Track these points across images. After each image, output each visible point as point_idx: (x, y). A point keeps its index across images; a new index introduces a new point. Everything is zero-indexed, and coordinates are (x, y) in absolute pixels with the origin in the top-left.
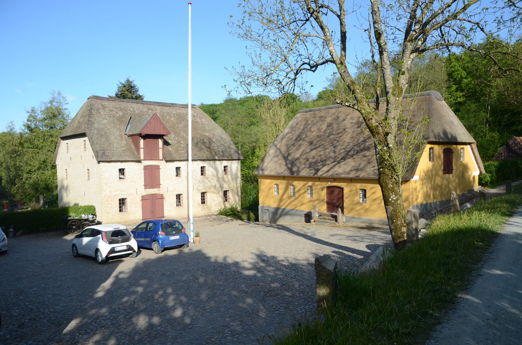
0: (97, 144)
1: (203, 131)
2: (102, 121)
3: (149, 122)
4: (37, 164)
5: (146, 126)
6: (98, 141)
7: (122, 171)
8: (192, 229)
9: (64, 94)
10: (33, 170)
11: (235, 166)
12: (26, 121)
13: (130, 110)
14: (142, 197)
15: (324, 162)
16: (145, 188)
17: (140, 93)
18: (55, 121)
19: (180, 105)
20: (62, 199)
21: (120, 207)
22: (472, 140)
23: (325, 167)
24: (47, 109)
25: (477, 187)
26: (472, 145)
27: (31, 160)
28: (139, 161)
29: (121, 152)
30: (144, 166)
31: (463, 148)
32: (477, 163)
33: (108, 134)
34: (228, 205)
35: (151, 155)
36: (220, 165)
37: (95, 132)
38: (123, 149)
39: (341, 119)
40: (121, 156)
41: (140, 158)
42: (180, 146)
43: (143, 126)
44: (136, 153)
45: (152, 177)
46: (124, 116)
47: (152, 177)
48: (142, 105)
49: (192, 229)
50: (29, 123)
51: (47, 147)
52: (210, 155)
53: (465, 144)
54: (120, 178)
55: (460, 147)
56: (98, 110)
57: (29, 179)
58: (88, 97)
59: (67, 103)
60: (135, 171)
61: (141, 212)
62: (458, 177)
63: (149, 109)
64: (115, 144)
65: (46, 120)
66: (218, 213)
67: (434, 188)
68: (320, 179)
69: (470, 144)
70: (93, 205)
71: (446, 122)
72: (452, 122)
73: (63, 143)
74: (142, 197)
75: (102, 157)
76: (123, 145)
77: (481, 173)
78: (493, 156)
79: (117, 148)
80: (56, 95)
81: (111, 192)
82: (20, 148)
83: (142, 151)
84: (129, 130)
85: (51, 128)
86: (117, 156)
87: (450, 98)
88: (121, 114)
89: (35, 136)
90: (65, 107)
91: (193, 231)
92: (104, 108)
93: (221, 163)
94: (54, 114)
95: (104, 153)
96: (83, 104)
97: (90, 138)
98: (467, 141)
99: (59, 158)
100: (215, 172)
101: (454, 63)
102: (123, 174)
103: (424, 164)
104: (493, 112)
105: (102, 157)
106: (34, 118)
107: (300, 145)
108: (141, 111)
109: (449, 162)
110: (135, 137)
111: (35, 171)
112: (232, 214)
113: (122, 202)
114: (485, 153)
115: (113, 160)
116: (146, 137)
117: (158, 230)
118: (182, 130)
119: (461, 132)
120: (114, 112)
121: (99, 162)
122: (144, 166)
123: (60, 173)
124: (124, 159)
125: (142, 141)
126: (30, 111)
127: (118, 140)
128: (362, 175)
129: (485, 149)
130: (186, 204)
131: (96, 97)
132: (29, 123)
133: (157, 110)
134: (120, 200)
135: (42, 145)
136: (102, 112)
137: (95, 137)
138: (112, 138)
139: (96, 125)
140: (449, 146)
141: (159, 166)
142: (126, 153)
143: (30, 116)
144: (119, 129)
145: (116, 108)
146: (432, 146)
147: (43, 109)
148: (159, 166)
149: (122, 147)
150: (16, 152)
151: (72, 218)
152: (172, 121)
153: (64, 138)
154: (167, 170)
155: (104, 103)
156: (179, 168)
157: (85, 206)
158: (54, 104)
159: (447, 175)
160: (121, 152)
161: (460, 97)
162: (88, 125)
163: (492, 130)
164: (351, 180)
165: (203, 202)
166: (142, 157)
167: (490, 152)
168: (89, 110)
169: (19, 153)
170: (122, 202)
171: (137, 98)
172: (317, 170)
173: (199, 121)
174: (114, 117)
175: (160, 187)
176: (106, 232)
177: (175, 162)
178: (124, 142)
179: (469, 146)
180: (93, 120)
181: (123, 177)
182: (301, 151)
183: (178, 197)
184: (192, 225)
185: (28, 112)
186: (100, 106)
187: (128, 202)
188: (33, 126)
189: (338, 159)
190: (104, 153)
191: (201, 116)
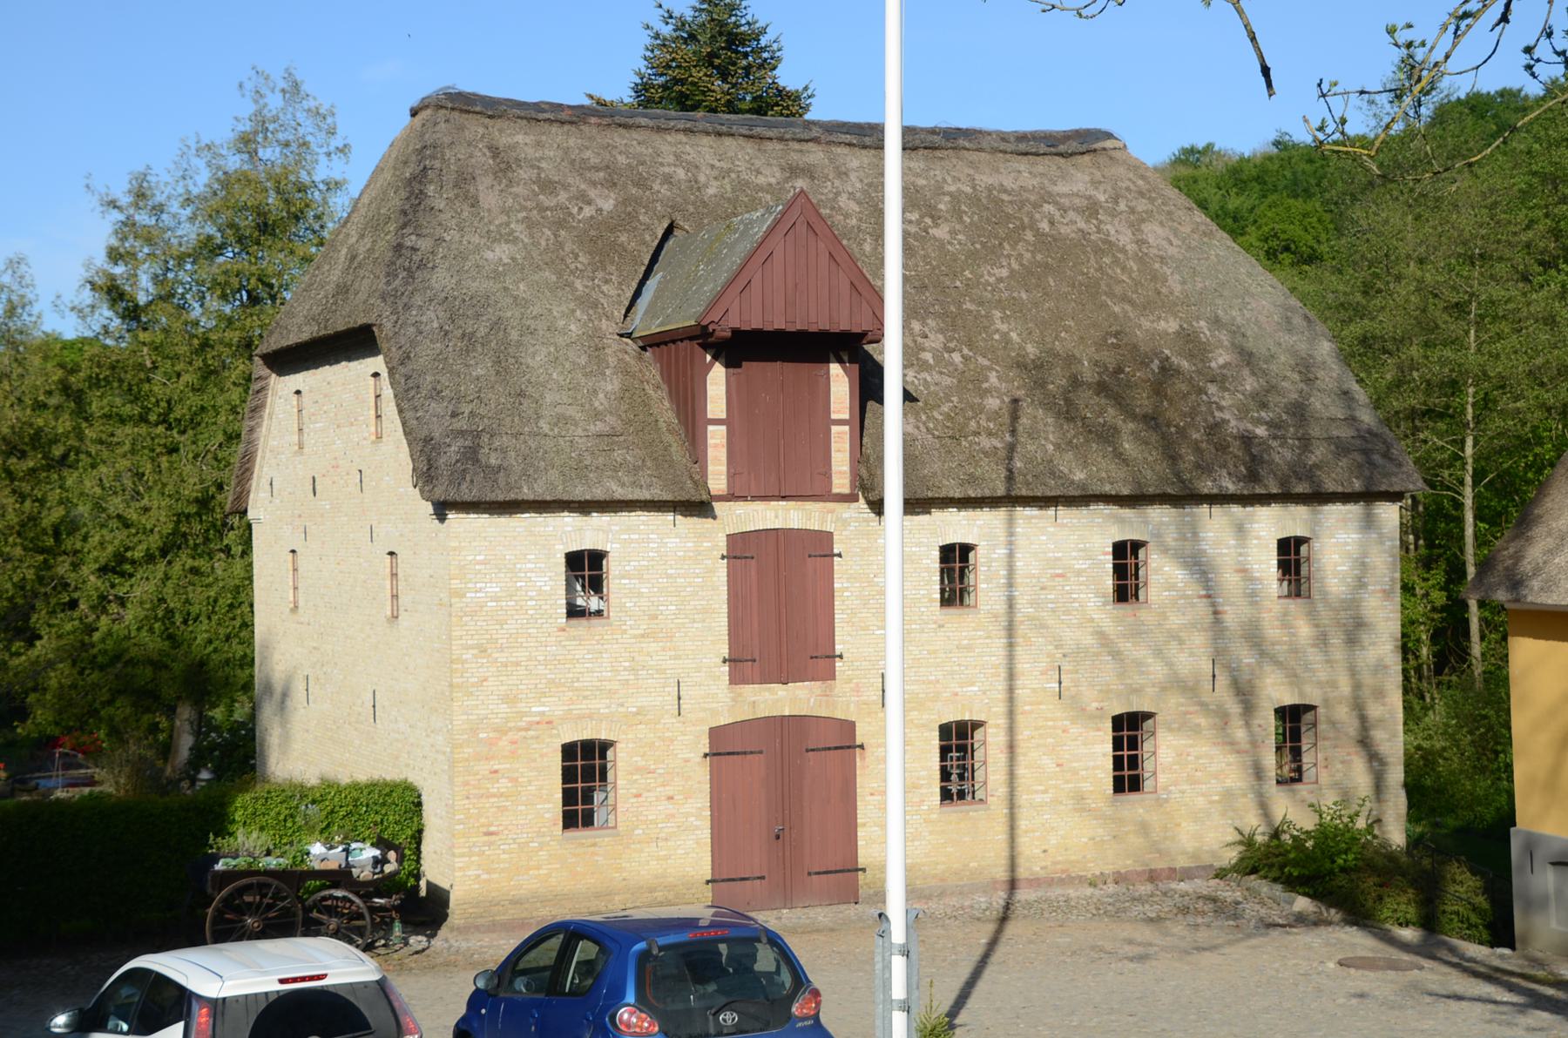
0: (436, 394)
1: (1146, 307)
2: (488, 248)
3: (760, 253)
4: (160, 518)
5: (739, 280)
6: (445, 380)
7: (586, 568)
8: (898, 991)
9: (320, 93)
10: (138, 554)
11: (1356, 547)
12: (101, 260)
13: (668, 179)
14: (715, 733)
16: (735, 679)
17: (787, 77)
18: (272, 259)
19: (1003, 137)
21: (569, 797)
24: (227, 182)
27: (109, 491)
28: (699, 507)
29: (582, 443)
30: (732, 539)
33: (514, 335)
34: (1296, 813)
35: (780, 465)
36: (1247, 539)
37: (433, 318)
38: (599, 427)
40: (581, 470)
41: (701, 482)
42: (979, 410)
43: (724, 277)
44: (677, 451)
45: (781, 609)
46: (625, 219)
47: (781, 609)
48: (750, 147)
49: (898, 991)
50: (119, 270)
51: (222, 419)
52: (1163, 468)
54: (574, 612)
56: (464, 179)
57: (114, 608)
58: (414, 101)
59: (344, 150)
60: (672, 569)
61: (706, 835)
63: (794, 171)
64: (549, 398)
65: (218, 250)
66: (1232, 856)
70: (414, 778)
73: (282, 388)
74: (715, 733)
75: (459, 477)
76: (600, 402)
79: (562, 420)
80: (274, 102)
81: (510, 699)
82: (64, 424)
83: (716, 437)
84: (651, 312)
85: (254, 300)
86: (553, 474)
88: (608, 205)
89: (156, 348)
90: (322, 171)
91: (906, 1007)
92: (504, 164)
93: (1240, 530)
94: (262, 218)
95: (472, 455)
96: (384, 148)
97: (396, 354)
99: (265, 483)
100: (1194, 590)
102: (596, 585)
105: (463, 478)
106: (149, 241)
108: (742, 185)
110: (684, 347)
111: (150, 558)
112: (1319, 874)
113: (585, 767)
115: (526, 493)
116: (740, 348)
117: (617, 998)
118: (999, 304)
120: (563, 197)
121: (442, 509)
122: (732, 539)
123: (1548, 503)
124: (598, 494)
125: (717, 378)
126: (125, 200)
127: (571, 364)
130: (1002, 791)
131: (461, 103)
132: (119, 270)
133: (842, 174)
134: (569, 751)
135: (194, 400)
136: (489, 198)
137: (426, 352)
138: (537, 358)
139: (441, 279)
141: (827, 537)
142: (618, 455)
143: (128, 227)
144: (590, 303)
145: (582, 167)
147: (202, 180)
148: (827, 537)
149: (597, 416)
150: (38, 440)
151: (241, 862)
152: (942, 245)
153: (291, 359)
154: (882, 561)
155: (503, 141)
156: (966, 549)
157: (356, 786)
158: (266, 153)
160: (582, 443)
162: (392, 275)
165: (1128, 778)
166: (717, 480)
168: (409, 182)
169: (57, 451)
170: (585, 767)
171: (761, 107)
173: (1125, 239)
174: (560, 224)
175: (831, 675)
176: (218, 1007)
177: (937, 515)
178: (612, 385)
180: (424, 245)
181: (594, 603)
183: (957, 741)
184: (898, 964)
185: (113, 204)
186: (482, 158)
187: (621, 763)
188: (144, 290)
190: (472, 455)
191: (1142, 205)
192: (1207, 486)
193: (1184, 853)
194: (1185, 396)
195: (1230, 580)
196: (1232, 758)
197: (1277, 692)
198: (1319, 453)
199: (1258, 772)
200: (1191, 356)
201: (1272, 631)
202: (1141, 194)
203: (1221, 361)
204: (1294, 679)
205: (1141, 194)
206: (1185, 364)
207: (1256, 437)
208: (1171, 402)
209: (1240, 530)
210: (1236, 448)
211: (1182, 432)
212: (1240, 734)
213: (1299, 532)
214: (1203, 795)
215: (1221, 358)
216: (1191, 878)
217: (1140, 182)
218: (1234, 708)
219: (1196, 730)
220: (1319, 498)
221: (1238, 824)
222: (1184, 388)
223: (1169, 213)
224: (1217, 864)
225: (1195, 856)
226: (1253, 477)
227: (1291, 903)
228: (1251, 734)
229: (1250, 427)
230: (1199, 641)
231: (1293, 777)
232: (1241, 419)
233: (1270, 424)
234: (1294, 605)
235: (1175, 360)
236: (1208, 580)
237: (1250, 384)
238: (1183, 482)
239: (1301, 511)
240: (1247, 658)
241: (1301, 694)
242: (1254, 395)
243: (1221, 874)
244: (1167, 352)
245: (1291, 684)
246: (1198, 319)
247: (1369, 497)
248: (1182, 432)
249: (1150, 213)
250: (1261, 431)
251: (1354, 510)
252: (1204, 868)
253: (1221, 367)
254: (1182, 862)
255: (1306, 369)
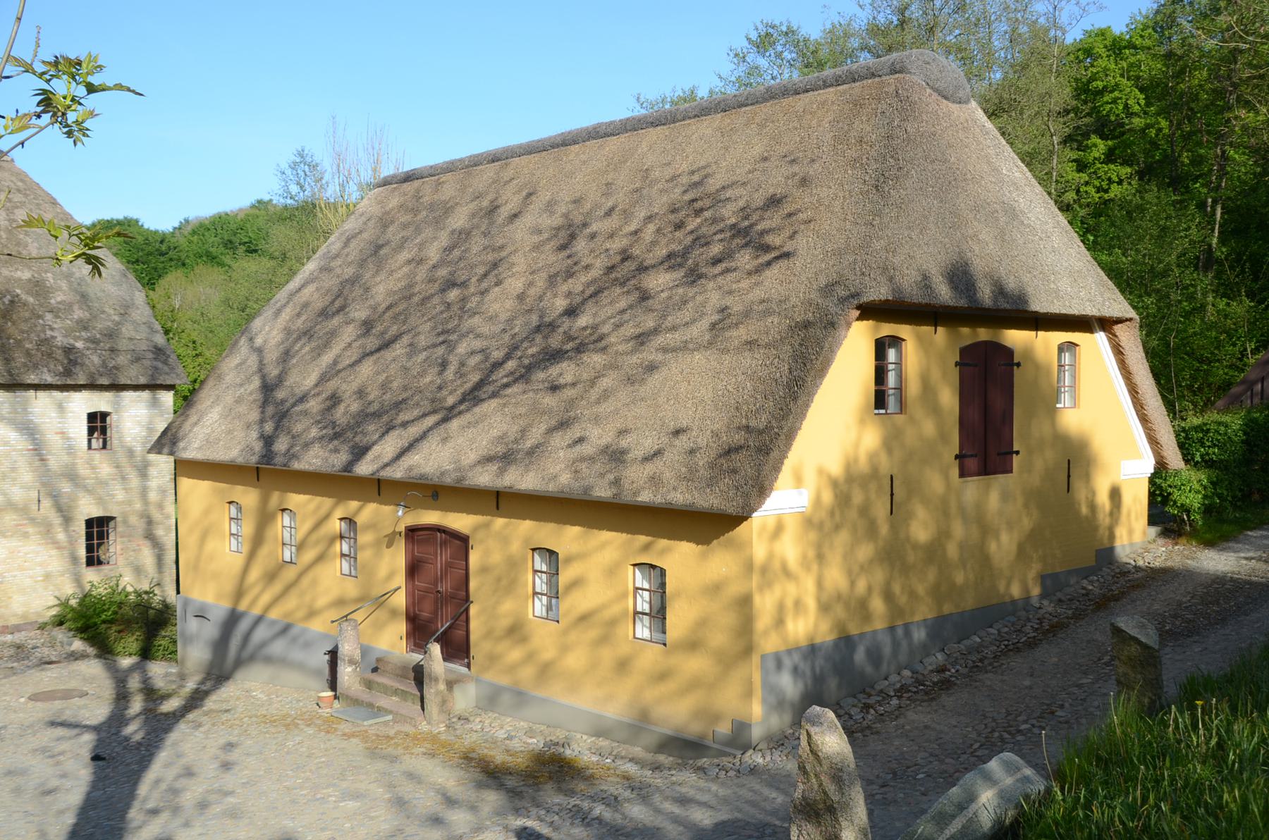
15: (384, 415)
20: (1048, 403)
22: (1115, 304)
23: (394, 434)
25: (1135, 539)
26: (1118, 329)
31: (1072, 345)
32: (1144, 420)
39: (504, 212)
53: (1082, 324)
55: (1046, 343)
62: (1035, 498)
67: (893, 555)
68: (379, 488)
69: (1106, 324)
71: (976, 209)
72: (1013, 213)
77: (1161, 466)
78: (1226, 386)
87: (1087, 183)
93: (61, 408)
98: (1090, 310)
101: (1102, 63)
103: (835, 428)
104: (1235, 229)
107: (333, 334)
109: (992, 413)
114: (1177, 370)
119: (1062, 268)
128: (524, 480)
129: (1201, 361)
140: (983, 334)
146: (887, 329)
159: (972, 488)
161: (1120, 182)
163: (1227, 291)
164: (500, 501)
167: (1220, 373)
172: (360, 452)
179: (1100, 337)
182: (327, 358)
189: (451, 401)
192: (32, 378)
193: (15, 615)
194: (26, 321)
195: (53, 440)
196: (54, 552)
197: (88, 508)
198: (122, 360)
199: (74, 559)
200: (37, 295)
201: (83, 471)
202: (19, 191)
203: (59, 299)
204: (100, 501)
205: (19, 191)
206: (31, 300)
207: (74, 348)
208: (14, 323)
209: (61, 408)
210: (59, 354)
211: (19, 343)
212: (61, 536)
213: (104, 408)
214: (31, 577)
215: (58, 298)
216: (19, 631)
217: (20, 184)
218: (56, 520)
219: (26, 535)
220: (117, 387)
221: (57, 594)
222: (27, 315)
223: (38, 204)
224: (41, 620)
225: (24, 616)
226: (68, 373)
227: (70, 645)
228: (70, 536)
229: (72, 341)
230: (27, 476)
231: (93, 561)
232: (66, 336)
233: (87, 340)
234: (97, 456)
235: (24, 297)
236: (35, 439)
237: (78, 313)
238: (11, 375)
239: (108, 395)
240: (66, 488)
241: (105, 509)
242: (80, 321)
243: (42, 627)
244: (18, 291)
245: (98, 504)
246: (46, 272)
247: (153, 387)
248: (19, 343)
249: (23, 204)
250: (79, 345)
251: (146, 395)
252: (31, 624)
253: (59, 303)
254: (14, 621)
255: (125, 310)
